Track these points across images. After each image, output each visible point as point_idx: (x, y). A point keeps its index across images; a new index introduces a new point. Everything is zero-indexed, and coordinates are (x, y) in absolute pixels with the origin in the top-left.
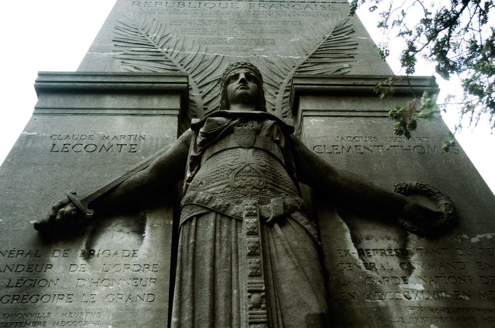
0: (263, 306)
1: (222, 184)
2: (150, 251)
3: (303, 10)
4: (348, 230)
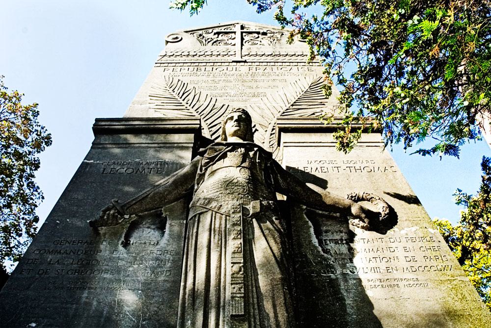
0: (241, 273)
1: (217, 192)
2: (168, 241)
3: (288, 71)
4: (312, 226)
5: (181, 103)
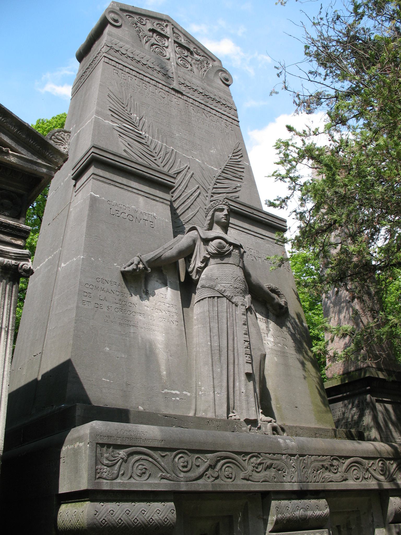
5: (140, 134)
